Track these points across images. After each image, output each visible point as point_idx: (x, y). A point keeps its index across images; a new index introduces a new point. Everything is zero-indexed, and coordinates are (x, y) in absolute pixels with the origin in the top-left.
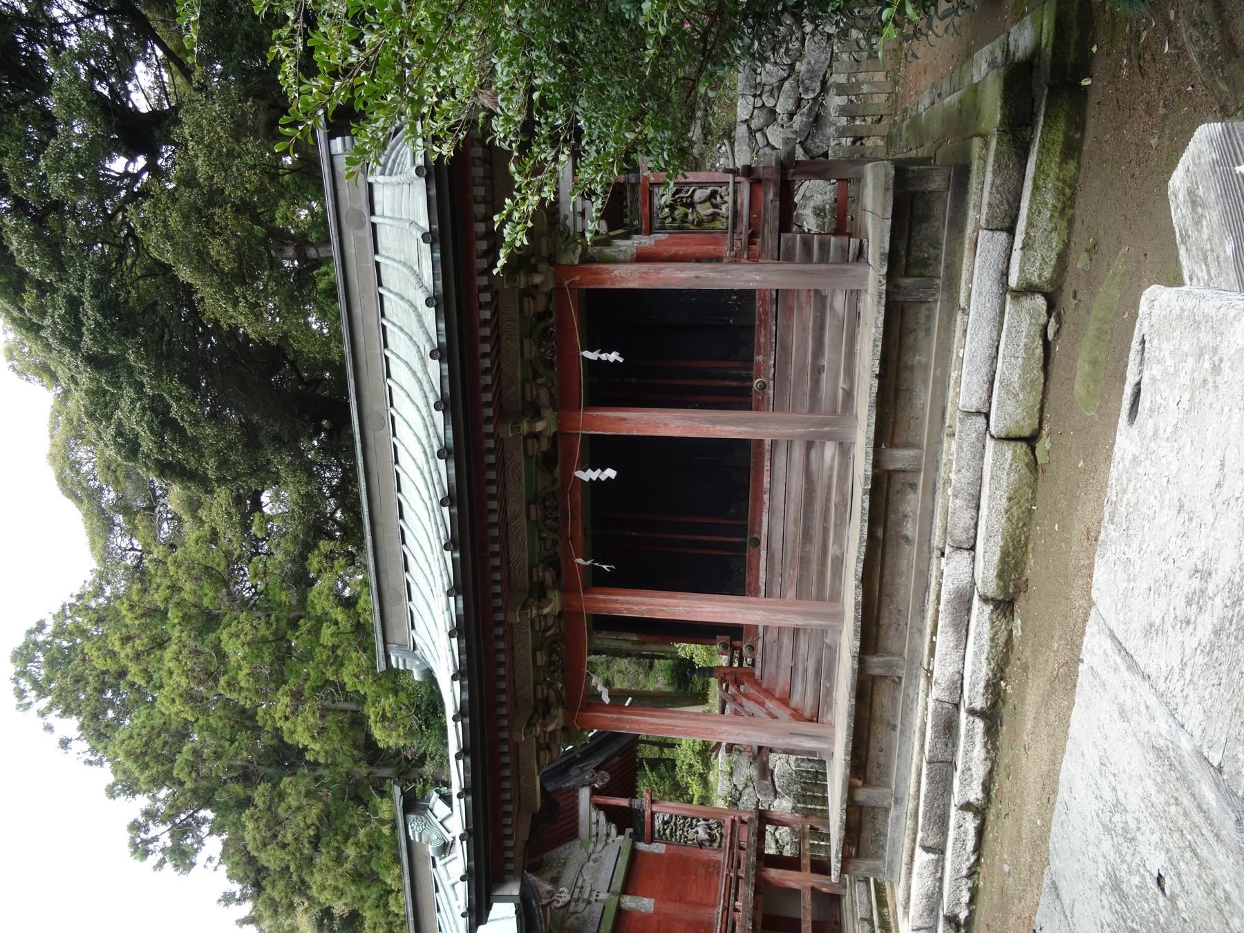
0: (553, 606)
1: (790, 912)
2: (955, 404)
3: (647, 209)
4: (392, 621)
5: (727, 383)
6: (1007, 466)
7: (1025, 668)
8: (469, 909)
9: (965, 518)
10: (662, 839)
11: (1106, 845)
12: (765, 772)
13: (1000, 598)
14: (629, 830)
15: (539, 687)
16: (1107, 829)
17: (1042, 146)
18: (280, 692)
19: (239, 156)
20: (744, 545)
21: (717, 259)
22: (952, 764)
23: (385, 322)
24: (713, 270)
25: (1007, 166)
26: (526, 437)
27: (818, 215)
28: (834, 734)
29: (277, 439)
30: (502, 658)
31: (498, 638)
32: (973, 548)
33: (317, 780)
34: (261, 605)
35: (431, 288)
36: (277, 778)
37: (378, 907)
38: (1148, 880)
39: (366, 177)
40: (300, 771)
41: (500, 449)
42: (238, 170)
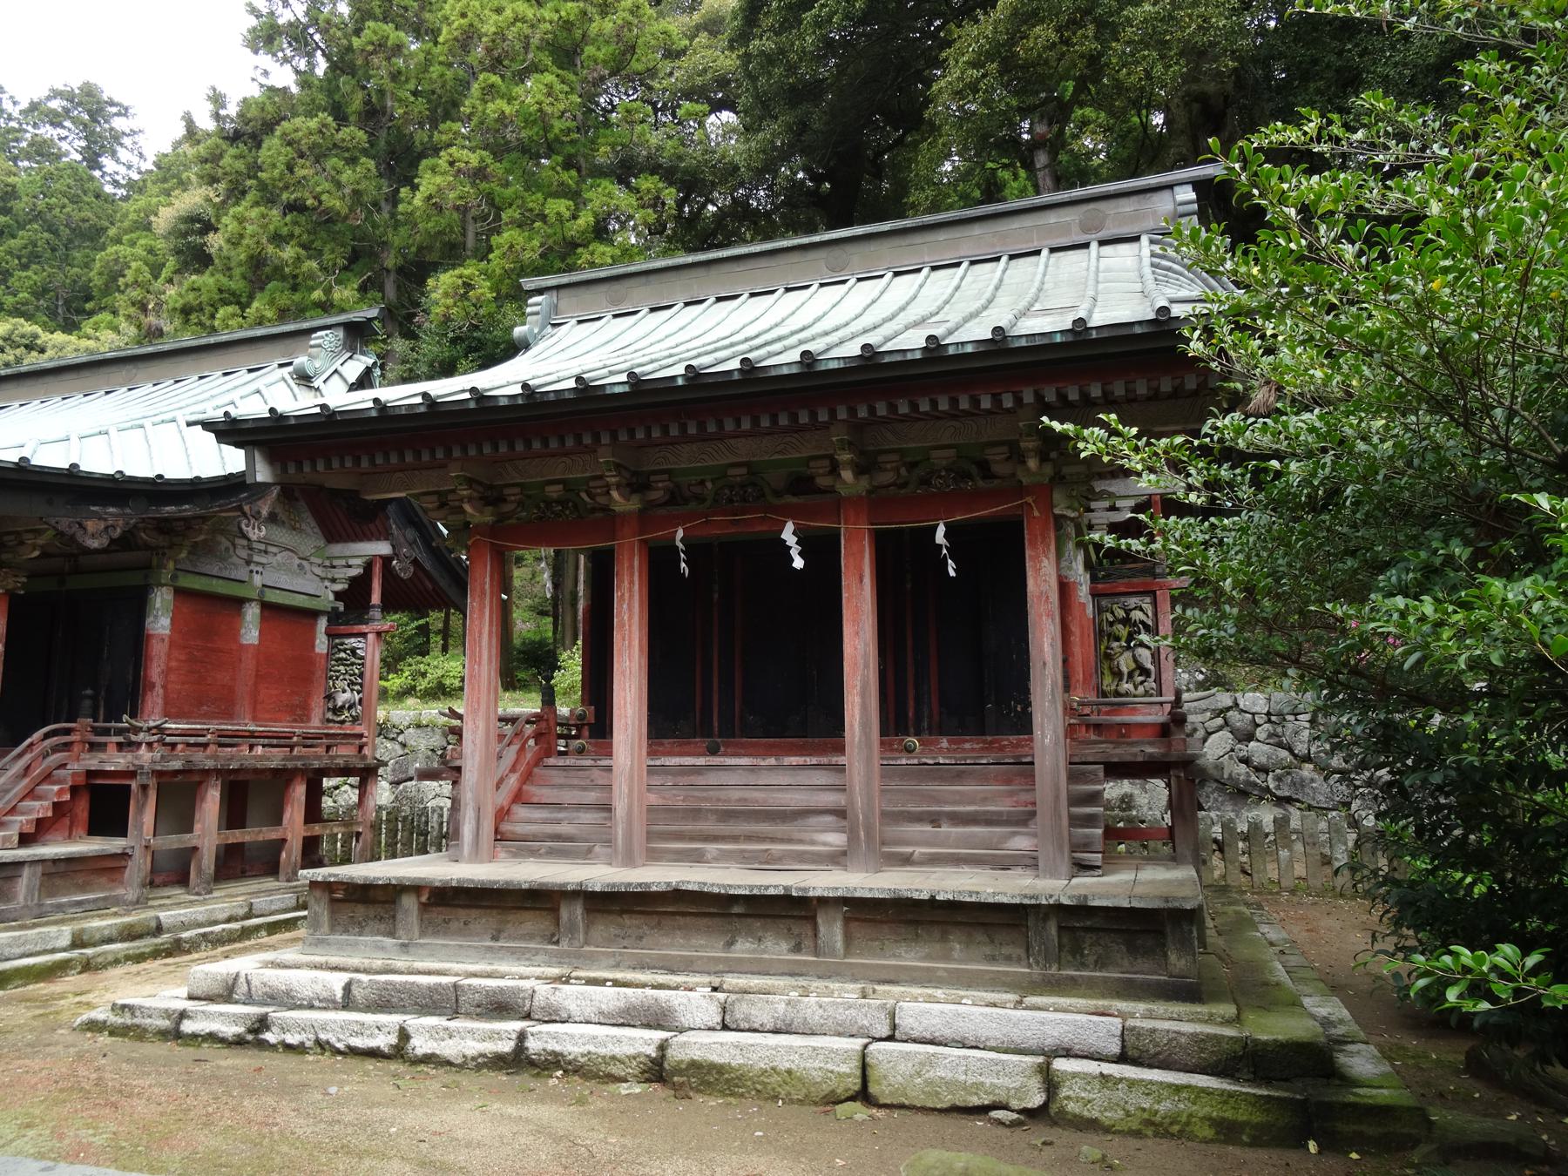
1: (253, 812)
3: (1123, 589)
4: (586, 294)
5: (911, 703)
6: (830, 1066)
7: (581, 1101)
8: (235, 421)
10: (333, 648)
13: (666, 1066)
14: (341, 606)
15: (516, 490)
17: (1231, 1095)
19: (1162, 57)
20: (710, 735)
21: (1067, 688)
22: (455, 1013)
23: (965, 265)
25: (1202, 1050)
26: (831, 458)
27: (1122, 800)
28: (482, 862)
29: (803, 127)
32: (725, 1027)
33: (375, 204)
34: (592, 119)
36: (373, 152)
39: (1148, 232)
40: (384, 182)
42: (1145, 58)
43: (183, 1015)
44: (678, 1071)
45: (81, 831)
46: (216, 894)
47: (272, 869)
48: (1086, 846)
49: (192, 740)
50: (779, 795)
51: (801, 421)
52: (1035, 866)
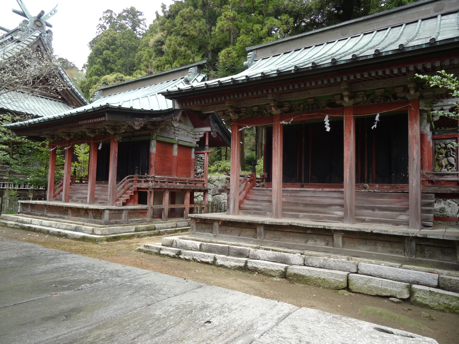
0: (275, 111)
1: (177, 201)
2: (361, 261)
3: (444, 137)
4: (265, 50)
6: (337, 279)
7: (263, 281)
9: (316, 263)
11: (217, 305)
12: (221, 191)
13: (287, 274)
15: (244, 109)
16: (223, 306)
18: (235, 12)
20: (301, 182)
21: (422, 168)
22: (228, 255)
24: (417, 166)
26: (341, 94)
27: (441, 209)
30: (255, 94)
31: (262, 91)
32: (305, 265)
35: (408, 46)
37: (166, 61)
38: (209, 318)
40: (208, 25)
41: (337, 84)
43: (161, 249)
44: (290, 275)
45: (136, 203)
46: (168, 221)
47: (182, 216)
48: (427, 220)
49: (162, 180)
50: (322, 200)
51: (331, 82)
52: (408, 225)
